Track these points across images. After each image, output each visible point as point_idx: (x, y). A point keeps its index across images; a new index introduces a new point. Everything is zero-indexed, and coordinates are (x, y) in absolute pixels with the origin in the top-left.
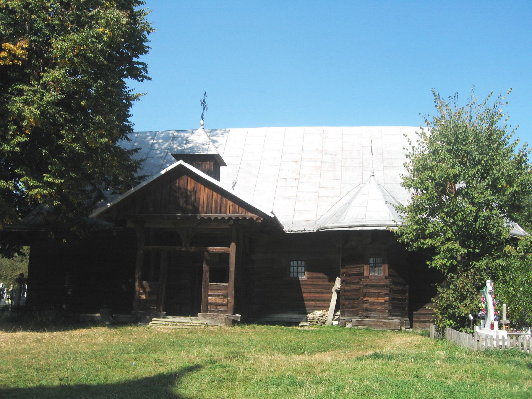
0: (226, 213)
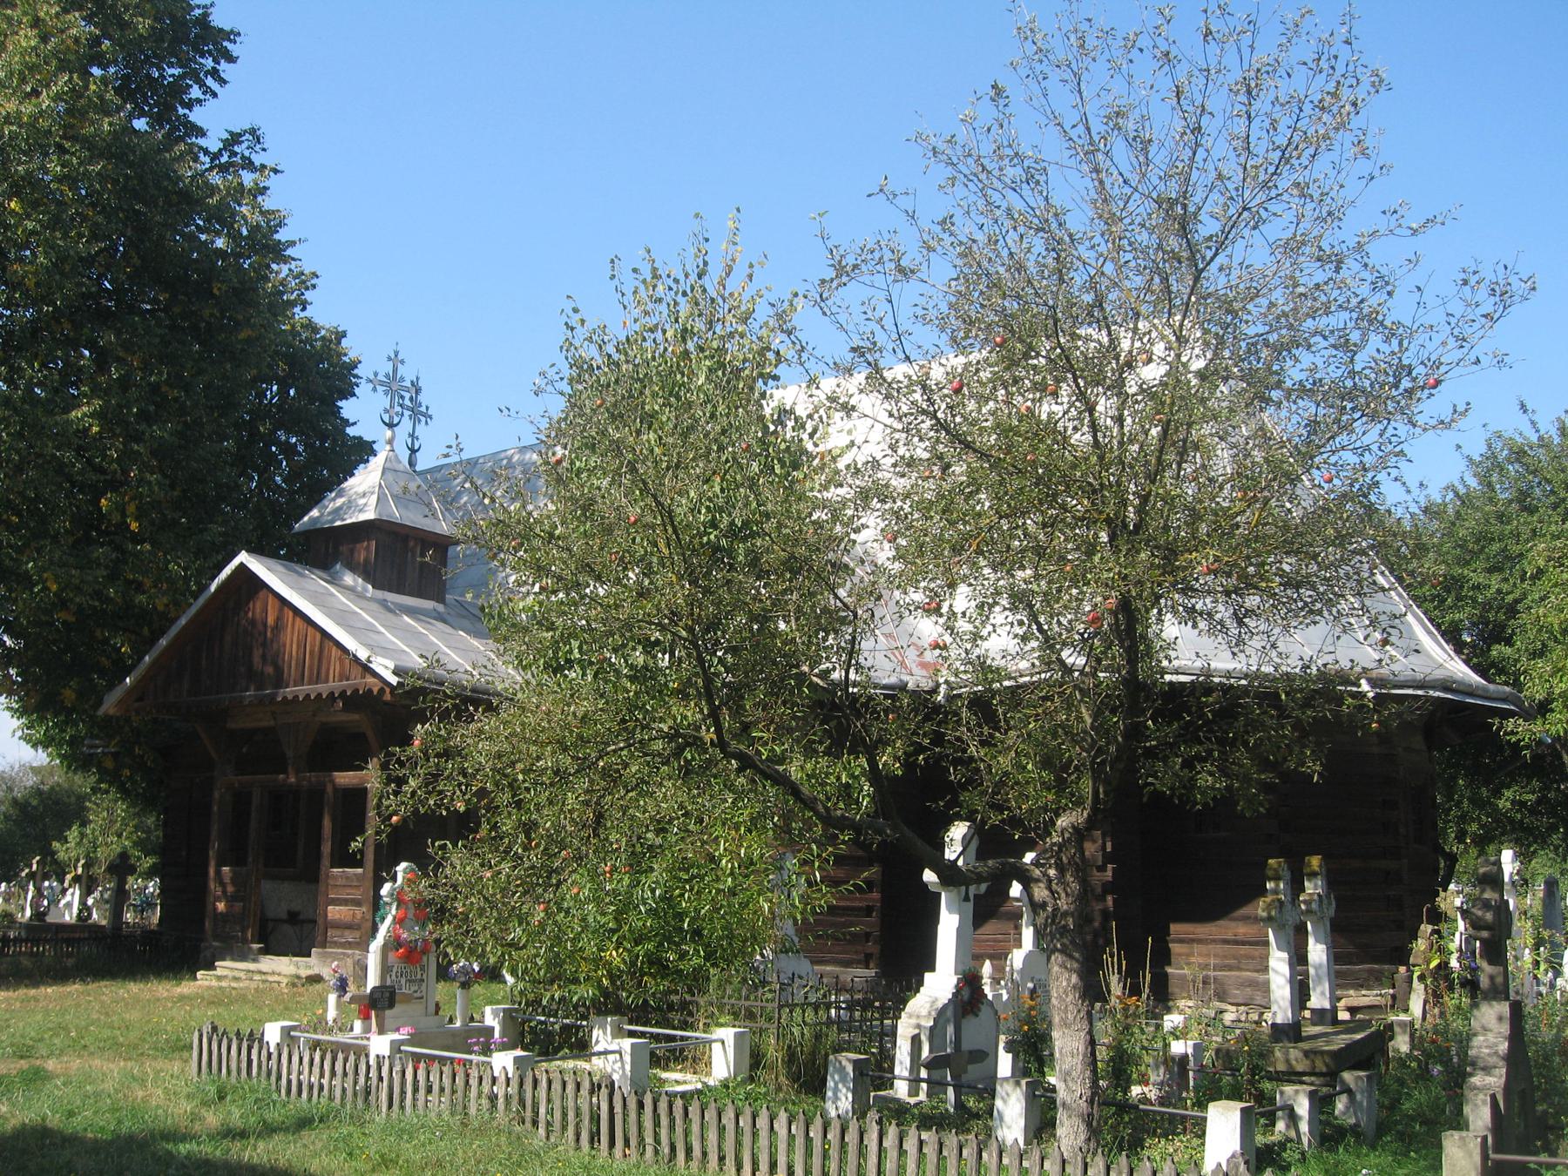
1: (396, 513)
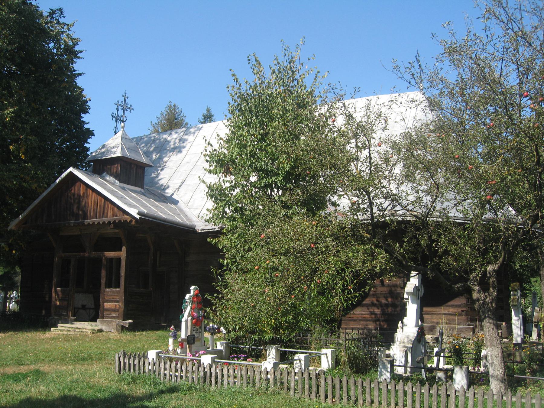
0: (107, 217)
1: (128, 154)
